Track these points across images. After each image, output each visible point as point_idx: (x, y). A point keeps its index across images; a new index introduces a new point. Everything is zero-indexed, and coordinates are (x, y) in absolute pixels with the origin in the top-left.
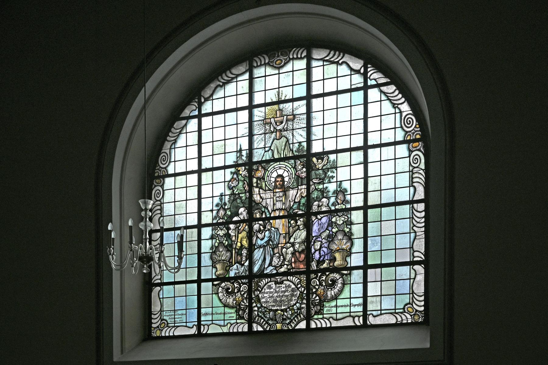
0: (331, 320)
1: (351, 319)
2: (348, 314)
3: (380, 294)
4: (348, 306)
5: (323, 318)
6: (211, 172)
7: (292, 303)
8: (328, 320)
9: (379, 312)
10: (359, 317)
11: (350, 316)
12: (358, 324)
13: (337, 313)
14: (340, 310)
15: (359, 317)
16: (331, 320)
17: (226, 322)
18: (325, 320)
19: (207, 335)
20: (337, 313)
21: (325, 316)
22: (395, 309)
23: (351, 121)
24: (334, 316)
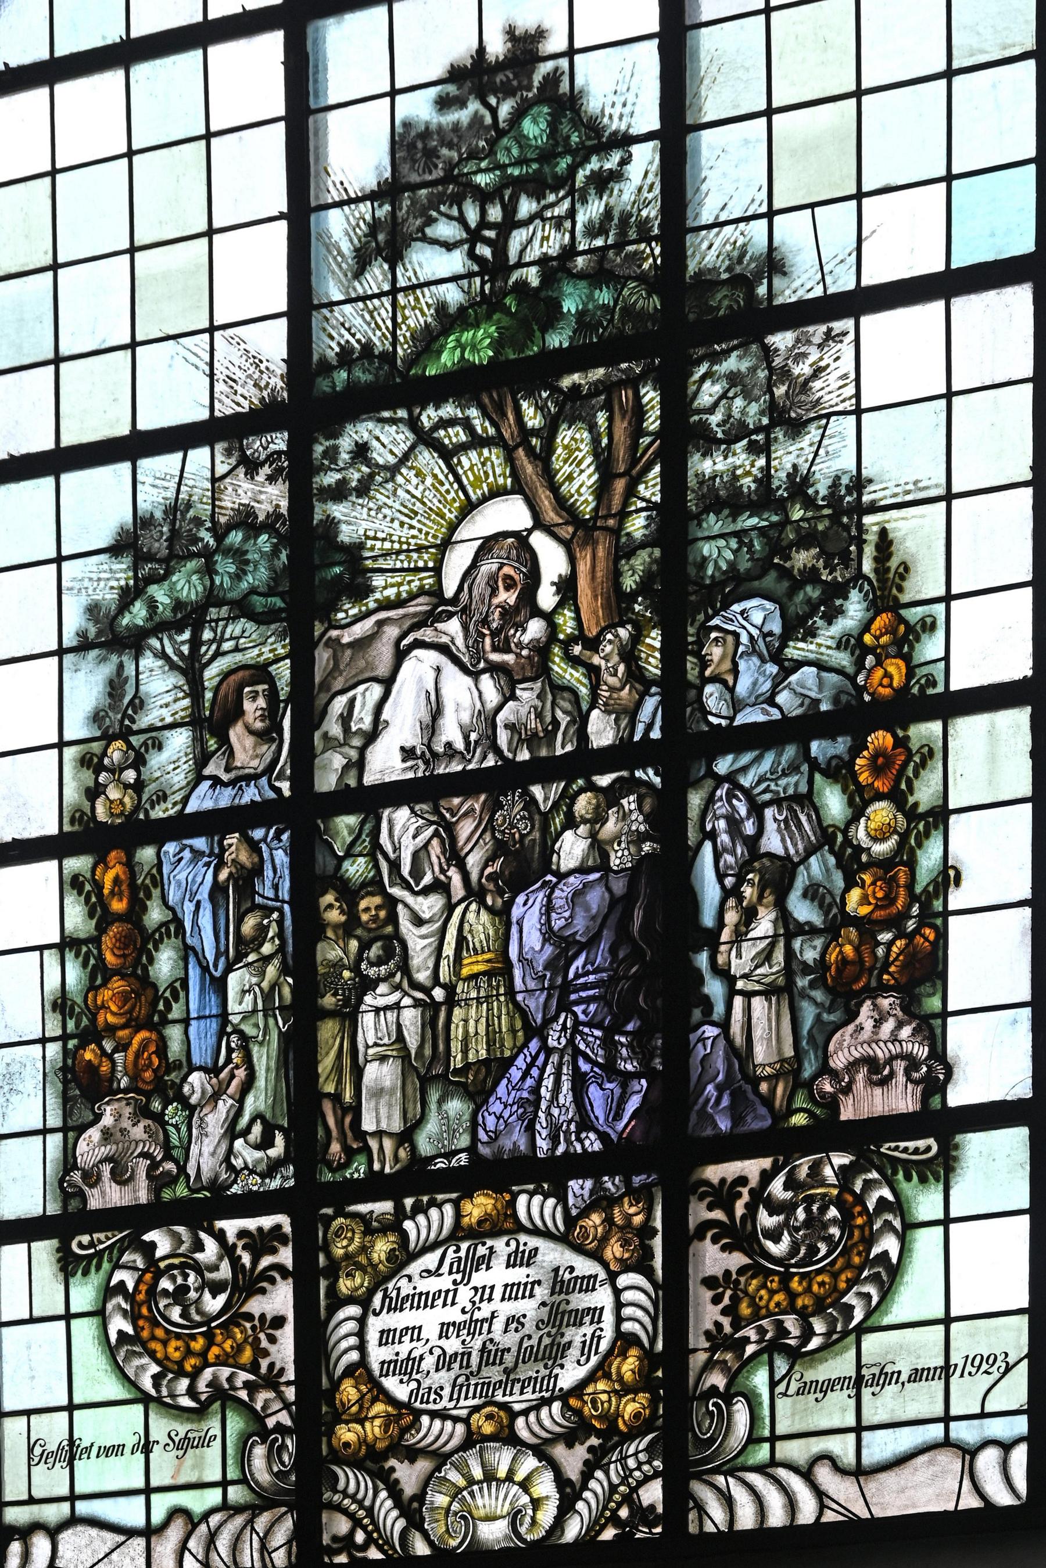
0: (824, 1475)
1: (951, 1463)
2: (936, 1431)
3: (140, 1484)
4: (875, 1381)
5: (773, 1462)
6: (42, 93)
7: (849, 1275)
8: (807, 1474)
9: (65, 1508)
10: (1006, 1447)
11: (947, 1443)
12: (1003, 1498)
13: (859, 1429)
14: (880, 1406)
15: (1006, 1447)
16: (824, 1475)
17: (162, 1504)
18: (754, 1478)
19: (514, 474)
20: (859, 1429)
21: (788, 1450)
22: (947, 1419)
23: (949, 178)
24: (843, 1447)
